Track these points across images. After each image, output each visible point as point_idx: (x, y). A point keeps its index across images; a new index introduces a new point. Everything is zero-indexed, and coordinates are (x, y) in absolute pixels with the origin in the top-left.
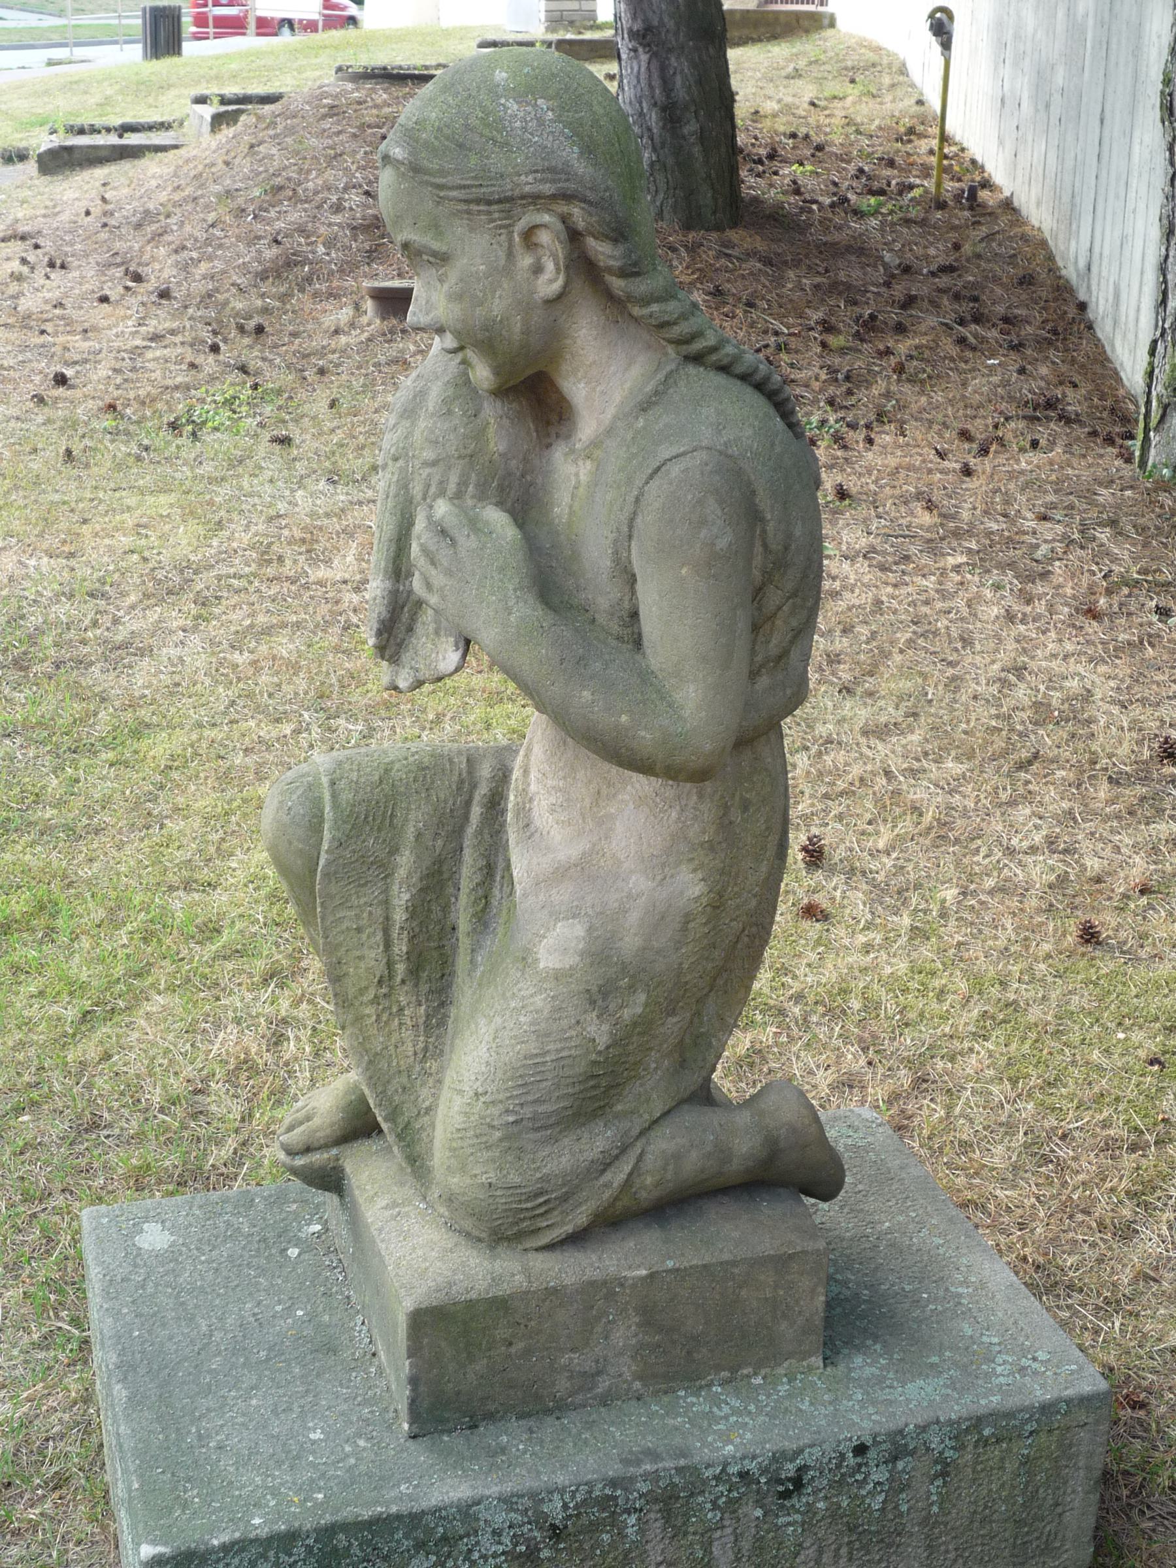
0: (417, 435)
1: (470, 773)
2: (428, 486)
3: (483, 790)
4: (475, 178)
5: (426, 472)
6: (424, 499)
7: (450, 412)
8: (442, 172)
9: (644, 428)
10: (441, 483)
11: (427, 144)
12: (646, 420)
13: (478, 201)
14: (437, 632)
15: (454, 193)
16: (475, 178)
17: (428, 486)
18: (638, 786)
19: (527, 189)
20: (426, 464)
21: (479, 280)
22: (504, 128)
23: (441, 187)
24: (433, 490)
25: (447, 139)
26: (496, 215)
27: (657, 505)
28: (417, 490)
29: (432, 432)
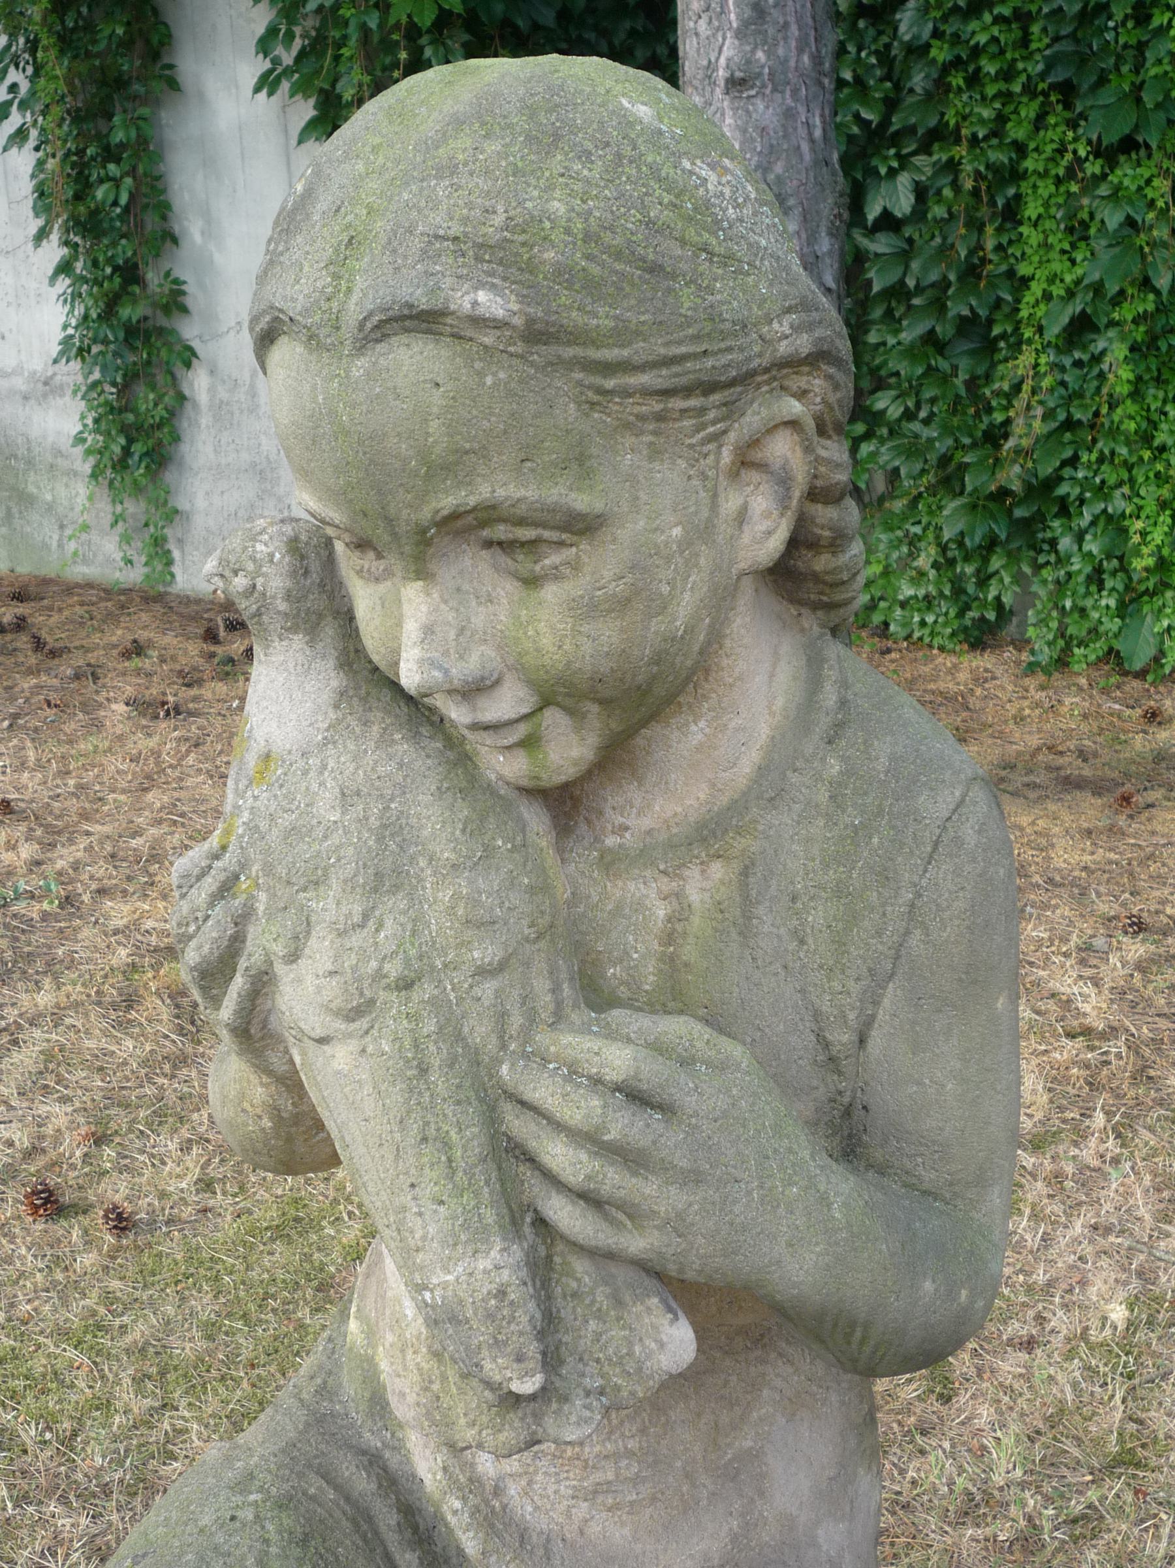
0: (436, 921)
1: (348, 1499)
2: (502, 1017)
3: (387, 1519)
4: (696, 338)
5: (488, 989)
6: (503, 1047)
7: (489, 851)
8: (622, 334)
9: (848, 773)
10: (524, 999)
11: (563, 274)
12: (844, 759)
13: (687, 391)
14: (619, 1303)
15: (644, 379)
16: (696, 338)
17: (502, 1017)
18: (778, 1383)
19: (783, 348)
20: (483, 972)
21: (668, 560)
22: (717, 222)
23: (608, 368)
24: (516, 1021)
25: (618, 255)
26: (712, 415)
27: (960, 904)
28: (479, 1031)
29: (477, 903)
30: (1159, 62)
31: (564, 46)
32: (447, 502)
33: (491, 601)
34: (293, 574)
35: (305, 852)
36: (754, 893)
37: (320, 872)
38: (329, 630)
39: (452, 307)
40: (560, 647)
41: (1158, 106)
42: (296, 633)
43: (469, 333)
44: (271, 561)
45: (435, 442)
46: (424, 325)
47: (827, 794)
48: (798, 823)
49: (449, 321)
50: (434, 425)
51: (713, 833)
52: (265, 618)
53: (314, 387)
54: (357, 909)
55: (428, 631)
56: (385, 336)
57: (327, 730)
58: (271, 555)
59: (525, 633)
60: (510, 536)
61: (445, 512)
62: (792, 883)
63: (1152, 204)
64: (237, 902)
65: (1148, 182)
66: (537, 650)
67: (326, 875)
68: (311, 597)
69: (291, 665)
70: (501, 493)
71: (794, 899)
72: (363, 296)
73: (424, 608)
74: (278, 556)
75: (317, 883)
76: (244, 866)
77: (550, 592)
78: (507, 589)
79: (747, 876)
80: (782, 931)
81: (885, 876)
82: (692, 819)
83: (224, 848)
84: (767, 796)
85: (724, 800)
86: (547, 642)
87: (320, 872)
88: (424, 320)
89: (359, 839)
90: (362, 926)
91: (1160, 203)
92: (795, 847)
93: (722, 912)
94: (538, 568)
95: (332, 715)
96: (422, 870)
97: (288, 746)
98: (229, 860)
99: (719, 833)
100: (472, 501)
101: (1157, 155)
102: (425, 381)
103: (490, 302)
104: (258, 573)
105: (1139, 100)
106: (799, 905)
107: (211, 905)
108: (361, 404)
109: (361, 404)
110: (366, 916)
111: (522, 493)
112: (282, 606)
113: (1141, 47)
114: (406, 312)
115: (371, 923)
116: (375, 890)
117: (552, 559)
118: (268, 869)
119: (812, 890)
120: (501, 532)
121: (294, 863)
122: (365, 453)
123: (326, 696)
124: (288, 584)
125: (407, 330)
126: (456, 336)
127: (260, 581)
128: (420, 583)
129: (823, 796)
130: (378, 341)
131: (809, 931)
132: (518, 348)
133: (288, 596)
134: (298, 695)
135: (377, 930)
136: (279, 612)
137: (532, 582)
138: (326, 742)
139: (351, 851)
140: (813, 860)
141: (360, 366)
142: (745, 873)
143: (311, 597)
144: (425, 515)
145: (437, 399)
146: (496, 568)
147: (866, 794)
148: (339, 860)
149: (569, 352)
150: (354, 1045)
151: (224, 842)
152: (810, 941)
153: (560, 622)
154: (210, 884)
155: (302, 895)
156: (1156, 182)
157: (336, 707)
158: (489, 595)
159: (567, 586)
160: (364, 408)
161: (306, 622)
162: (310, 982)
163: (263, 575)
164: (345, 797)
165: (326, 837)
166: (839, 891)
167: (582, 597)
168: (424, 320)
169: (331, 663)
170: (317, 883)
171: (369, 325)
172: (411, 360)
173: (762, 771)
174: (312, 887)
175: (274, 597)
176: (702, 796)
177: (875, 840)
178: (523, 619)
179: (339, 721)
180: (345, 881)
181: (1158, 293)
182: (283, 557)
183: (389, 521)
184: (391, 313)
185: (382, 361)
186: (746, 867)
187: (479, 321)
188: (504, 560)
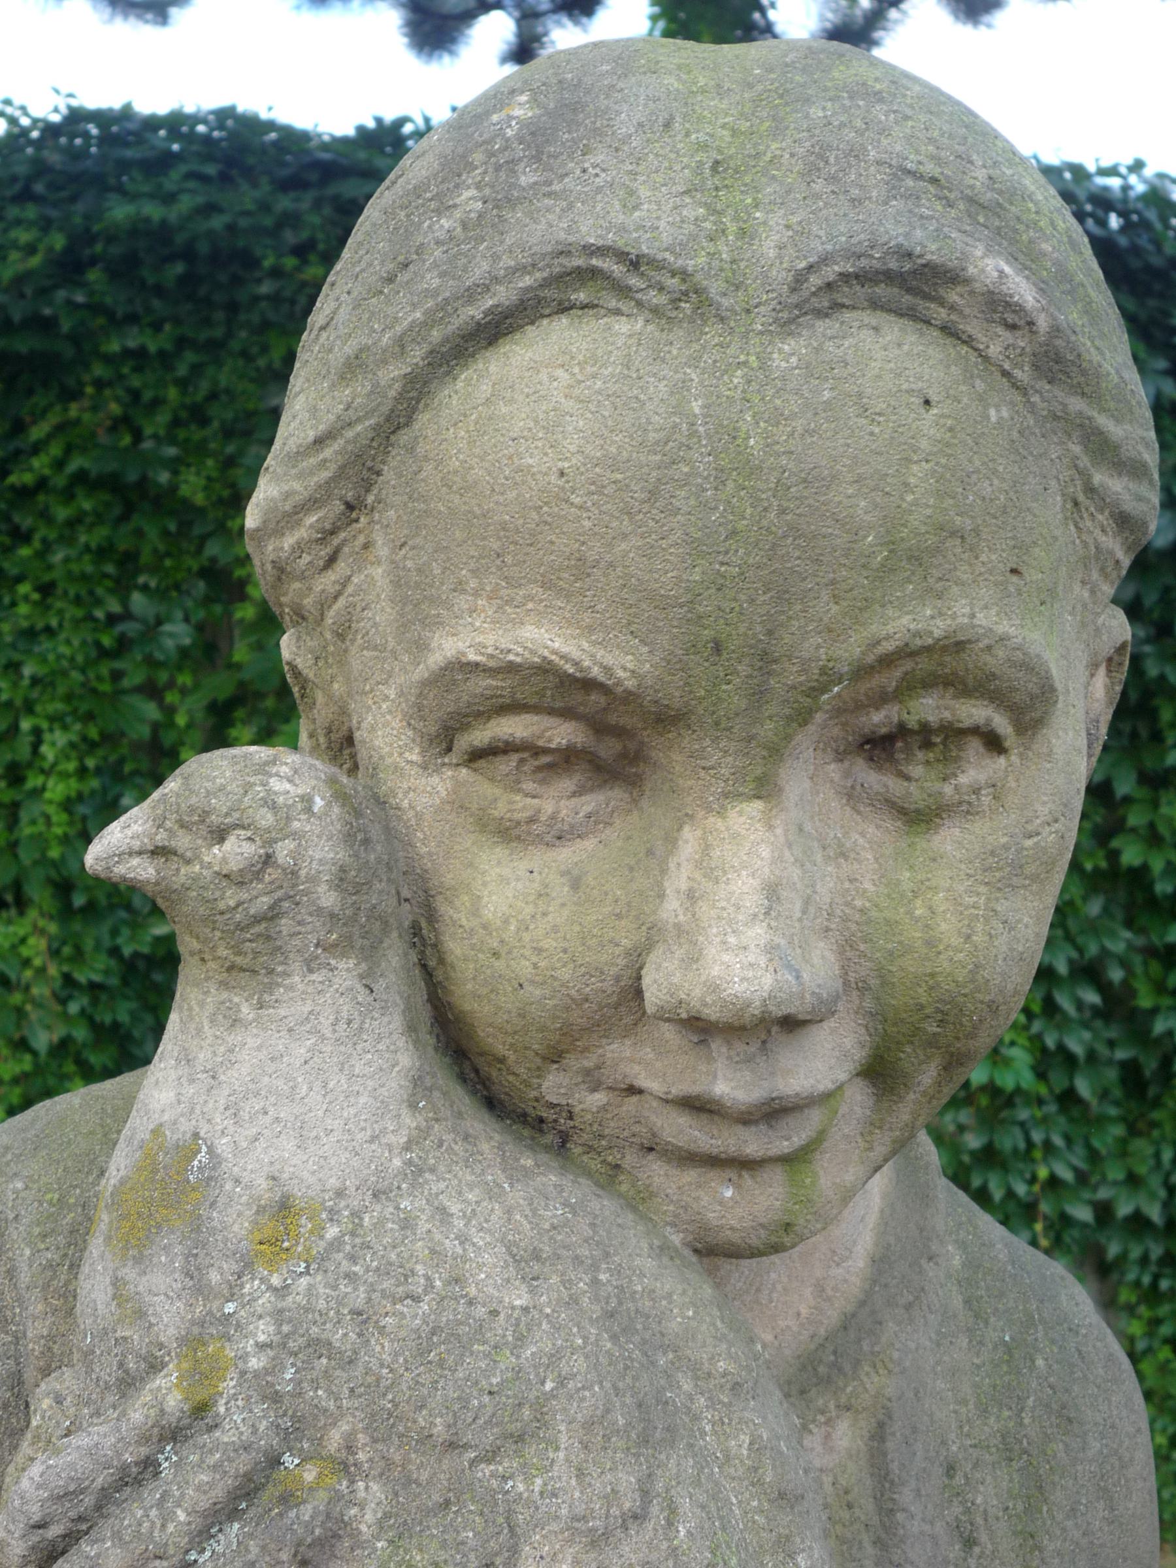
30: (33, 822)
31: (302, 300)
32: (905, 621)
33: (843, 855)
34: (349, 837)
35: (486, 1373)
36: (895, 1467)
37: (526, 1412)
38: (395, 956)
39: (971, 270)
40: (968, 937)
41: (36, 863)
42: (343, 955)
43: (972, 328)
44: (308, 810)
45: (915, 503)
46: (907, 299)
47: (960, 1298)
48: (938, 1345)
49: (953, 296)
50: (917, 471)
51: (836, 1366)
52: (285, 925)
53: (681, 388)
54: (627, 1480)
55: (772, 891)
56: (837, 306)
57: (407, 1148)
58: (307, 800)
59: (910, 913)
60: (947, 715)
61: (888, 646)
62: (944, 1443)
63: (26, 962)
64: (306, 1512)
65: (23, 941)
66: (929, 943)
67: (541, 1419)
68: (378, 886)
69: (325, 1023)
70: (981, 619)
71: (950, 1470)
72: (781, 235)
73: (765, 852)
74: (319, 803)
75: (520, 1439)
76: (298, 1428)
77: (950, 840)
78: (870, 836)
79: (882, 1440)
80: (939, 1528)
81: (1066, 1419)
82: (787, 1352)
83: (201, 1409)
84: (902, 1301)
85: (833, 1316)
86: (947, 928)
87: (526, 1412)
88: (911, 287)
89: (585, 1338)
90: (639, 1517)
91: (37, 962)
92: (940, 1385)
93: (850, 1506)
94: (948, 789)
95: (410, 1121)
96: (691, 1398)
97: (333, 1182)
98: (240, 1422)
99: (847, 1368)
100: (939, 628)
101: (33, 914)
102: (910, 392)
103: (1024, 291)
104: (283, 830)
105: (16, 856)
106: (959, 1480)
107: (202, 1536)
108: (793, 416)
109: (793, 416)
110: (646, 1494)
111: (1004, 627)
112: (328, 898)
113: (15, 806)
114: (893, 265)
115: (655, 1509)
116: (644, 1440)
117: (977, 769)
118: (383, 1425)
119: (975, 1453)
120: (929, 708)
121: (464, 1401)
122: (783, 511)
123: (395, 1085)
124: (342, 855)
125: (875, 305)
126: (948, 330)
127: (283, 851)
128: (758, 805)
129: (957, 1302)
130: (820, 314)
131: (979, 1520)
132: (1023, 375)
133: (341, 880)
134: (338, 1081)
135: (670, 1523)
136: (319, 911)
137: (918, 818)
138: (416, 1172)
139: (579, 1363)
140: (964, 1402)
141: (787, 355)
142: (879, 1434)
143: (378, 886)
144: (851, 649)
145: (928, 425)
146: (852, 796)
147: (1002, 1294)
148: (561, 1382)
149: (1076, 404)
151: (201, 1395)
152: (984, 1538)
153: (970, 892)
154: (192, 1481)
155: (485, 1469)
156: (32, 941)
157: (413, 1106)
158: (841, 845)
159: (979, 827)
160: (799, 424)
161: (353, 934)
163: (295, 835)
164: (526, 1262)
165: (520, 1339)
166: (1010, 1449)
167: (1006, 847)
168: (911, 287)
169: (395, 1022)
170: (520, 1439)
171: (815, 281)
172: (885, 354)
173: (881, 1262)
174: (510, 1446)
175: (313, 880)
176: (804, 1311)
177: (1040, 1362)
178: (907, 886)
179: (423, 1133)
180: (589, 1425)
181: (35, 1053)
182: (329, 804)
183: (766, 660)
184: (864, 262)
185: (830, 346)
186: (881, 1425)
187: (1000, 308)
188: (873, 779)
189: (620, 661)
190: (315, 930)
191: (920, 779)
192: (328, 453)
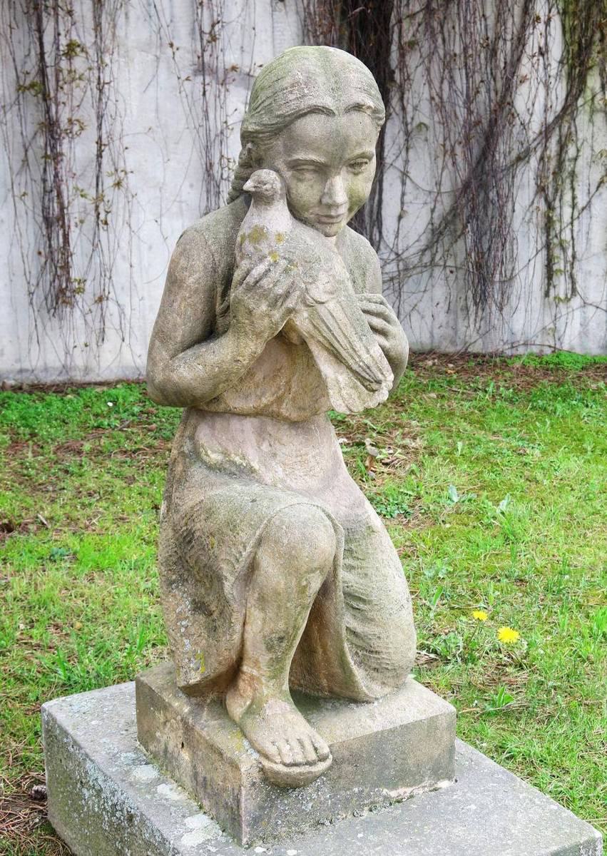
77: (360, 177)
137: (356, 174)
150: (335, 301)
162: (321, 287)
188: (350, 169)
189: (322, 160)
190: (278, 196)
191: (357, 170)
192: (260, 102)
